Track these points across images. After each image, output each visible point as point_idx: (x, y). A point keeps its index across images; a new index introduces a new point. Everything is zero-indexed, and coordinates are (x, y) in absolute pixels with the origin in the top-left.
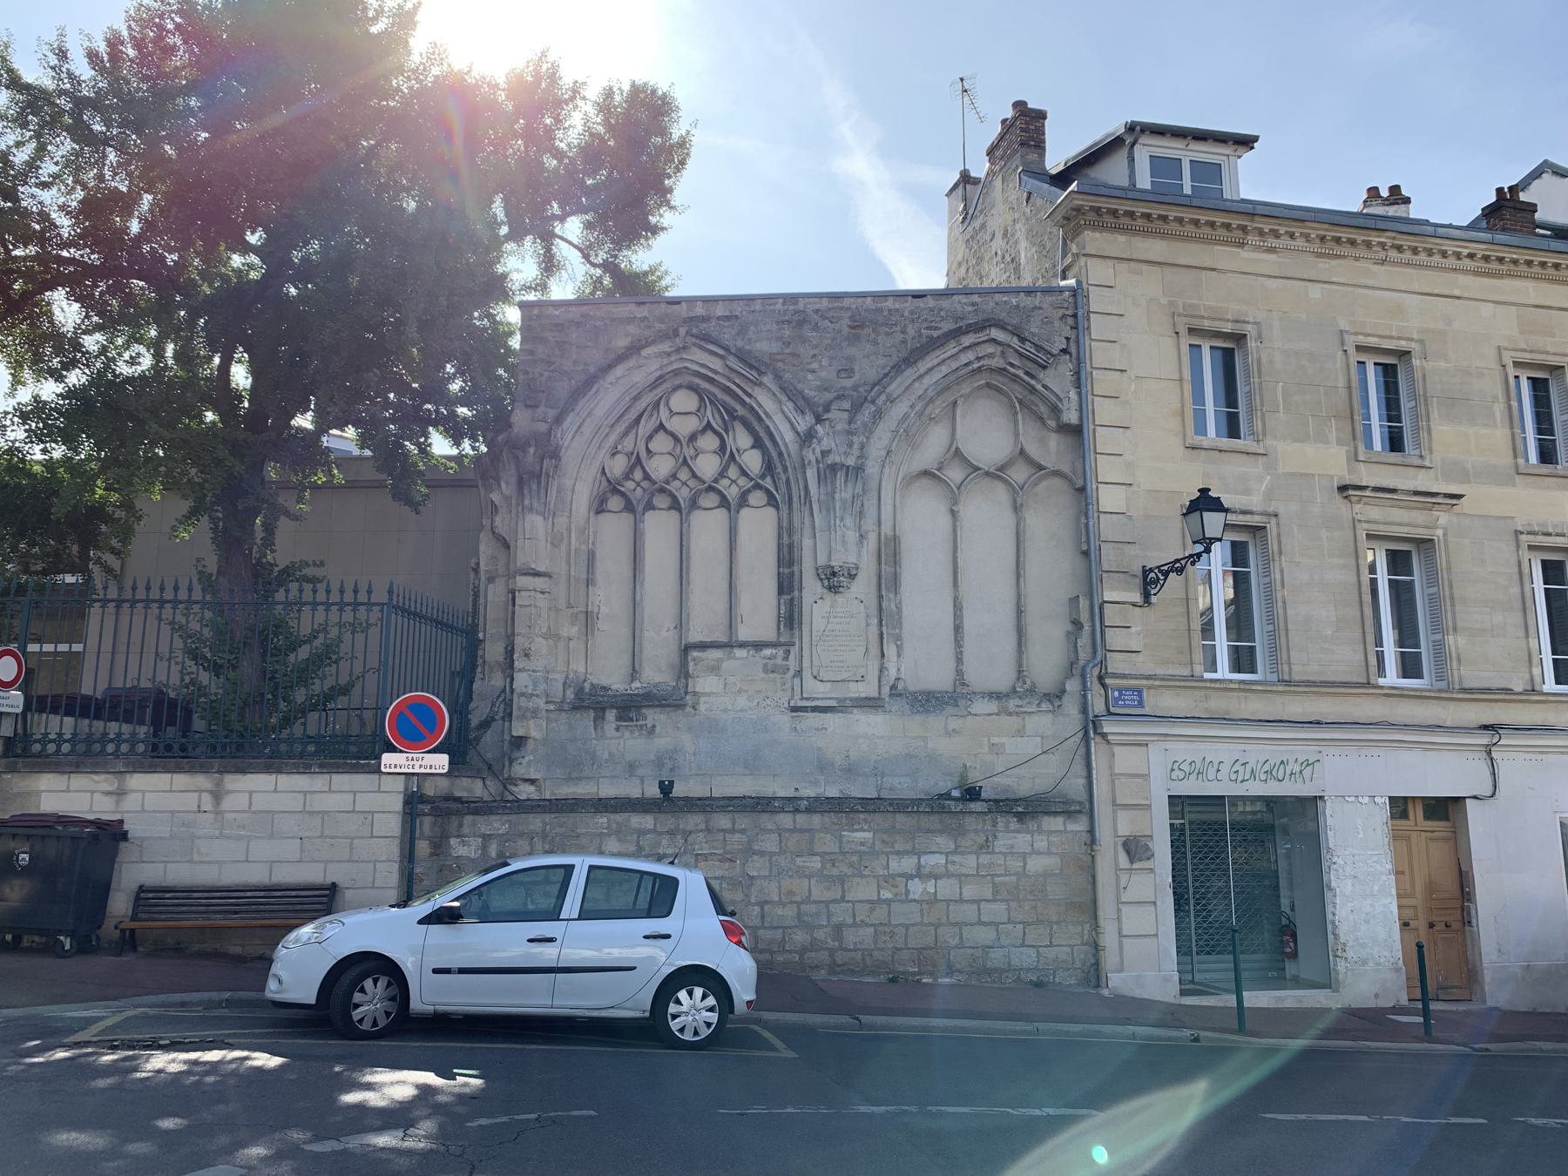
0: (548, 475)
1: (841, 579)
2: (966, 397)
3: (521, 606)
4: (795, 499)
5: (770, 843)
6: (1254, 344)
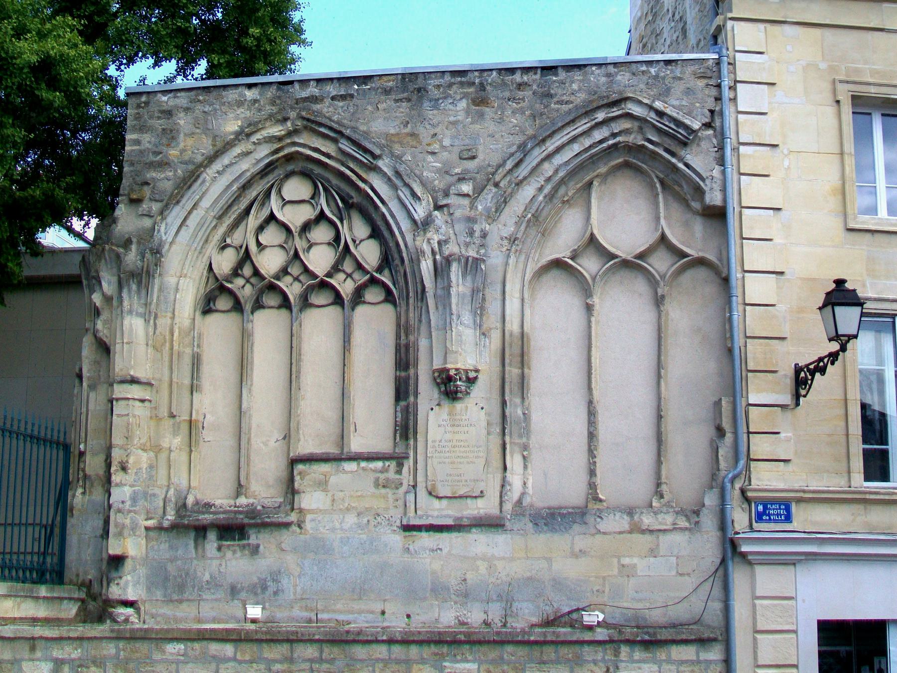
0: (148, 272)
2: (604, 177)
3: (118, 415)
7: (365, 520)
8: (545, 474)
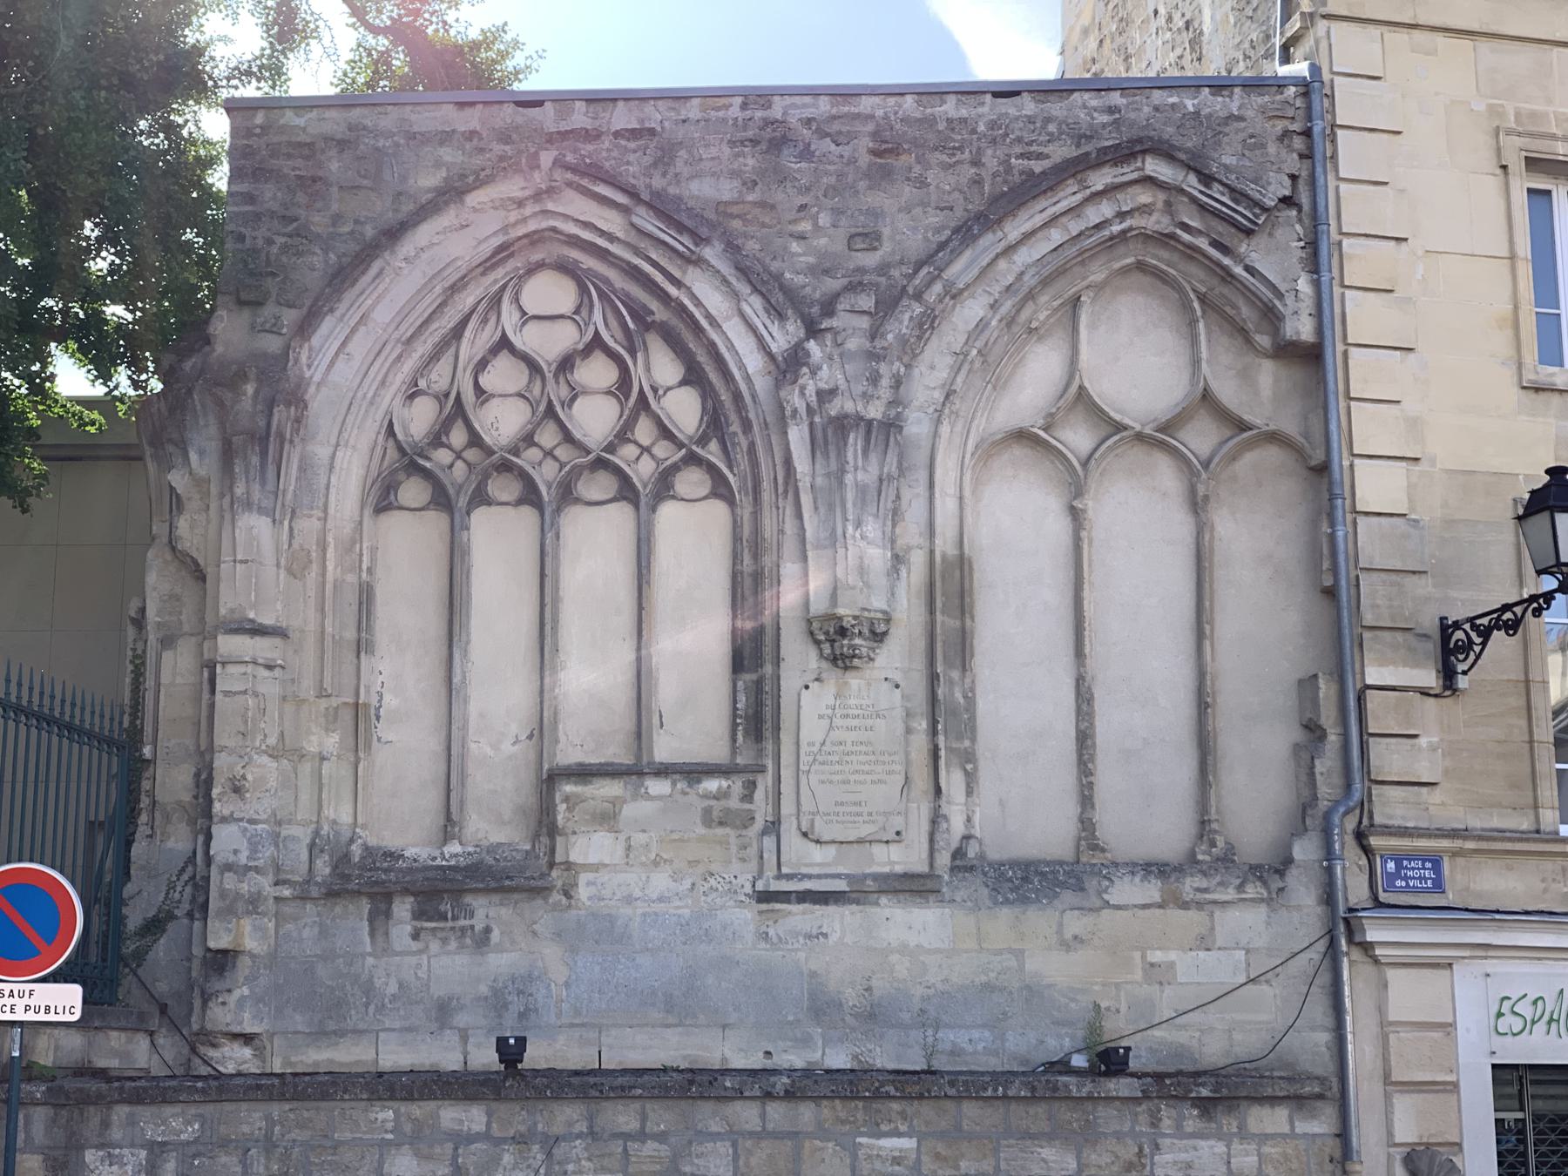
0: (281, 437)
1: (858, 641)
2: (1099, 288)
3: (227, 693)
7: (687, 884)
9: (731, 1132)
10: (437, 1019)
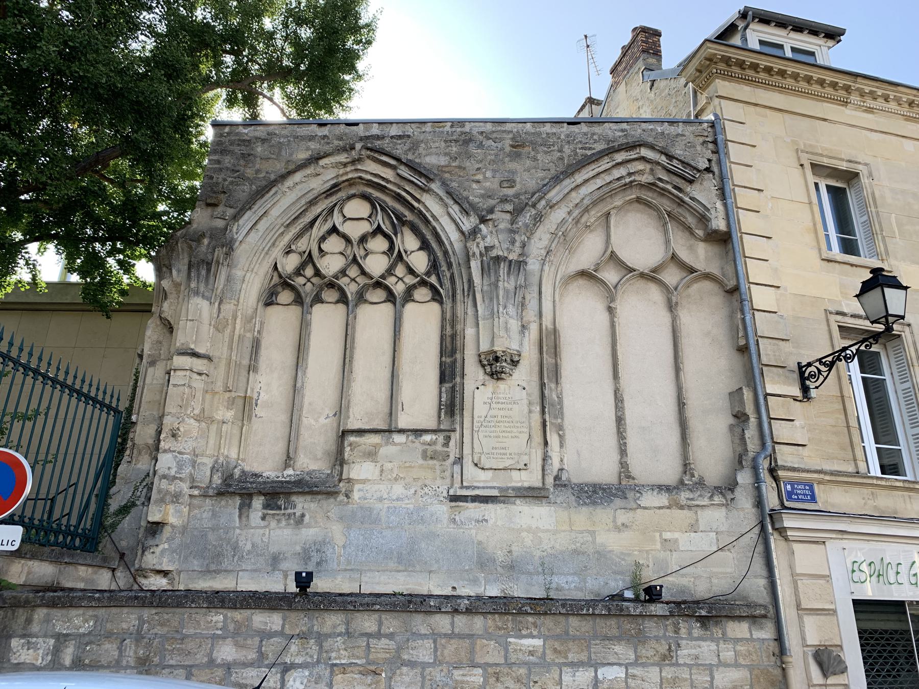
0: (218, 263)
1: (504, 364)
2: (619, 209)
3: (175, 385)
4: (459, 292)
5: (423, 652)
6: (867, 181)
7: (412, 491)
8: (579, 454)
9: (433, 634)
10: (271, 565)
